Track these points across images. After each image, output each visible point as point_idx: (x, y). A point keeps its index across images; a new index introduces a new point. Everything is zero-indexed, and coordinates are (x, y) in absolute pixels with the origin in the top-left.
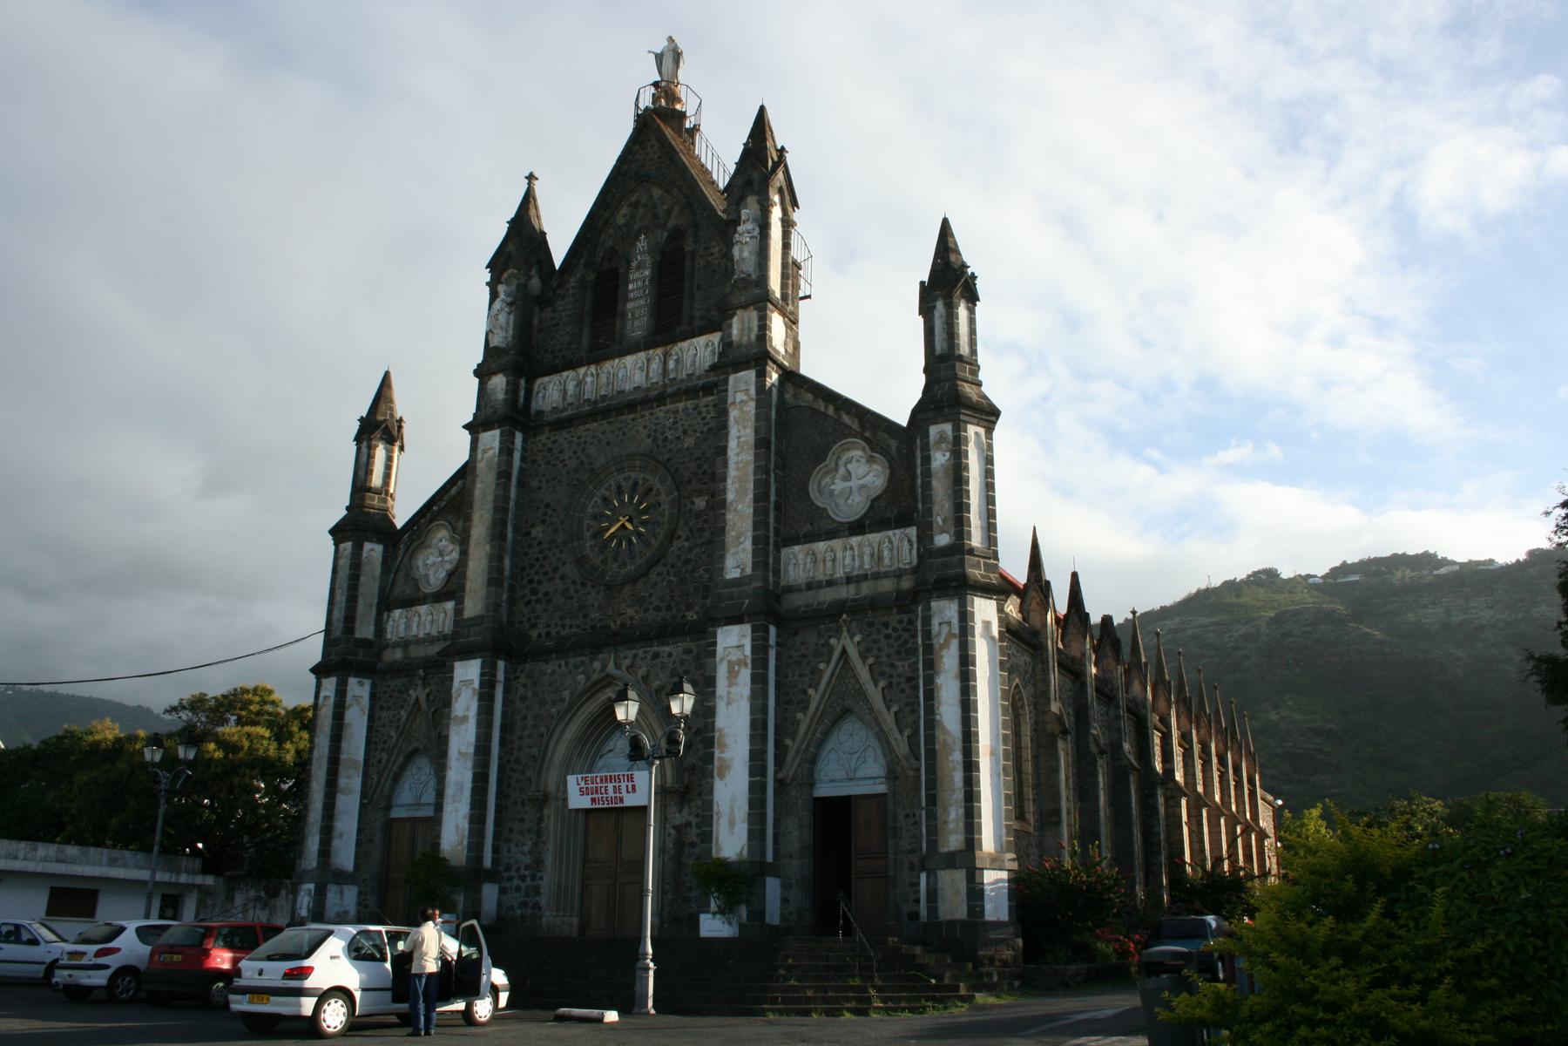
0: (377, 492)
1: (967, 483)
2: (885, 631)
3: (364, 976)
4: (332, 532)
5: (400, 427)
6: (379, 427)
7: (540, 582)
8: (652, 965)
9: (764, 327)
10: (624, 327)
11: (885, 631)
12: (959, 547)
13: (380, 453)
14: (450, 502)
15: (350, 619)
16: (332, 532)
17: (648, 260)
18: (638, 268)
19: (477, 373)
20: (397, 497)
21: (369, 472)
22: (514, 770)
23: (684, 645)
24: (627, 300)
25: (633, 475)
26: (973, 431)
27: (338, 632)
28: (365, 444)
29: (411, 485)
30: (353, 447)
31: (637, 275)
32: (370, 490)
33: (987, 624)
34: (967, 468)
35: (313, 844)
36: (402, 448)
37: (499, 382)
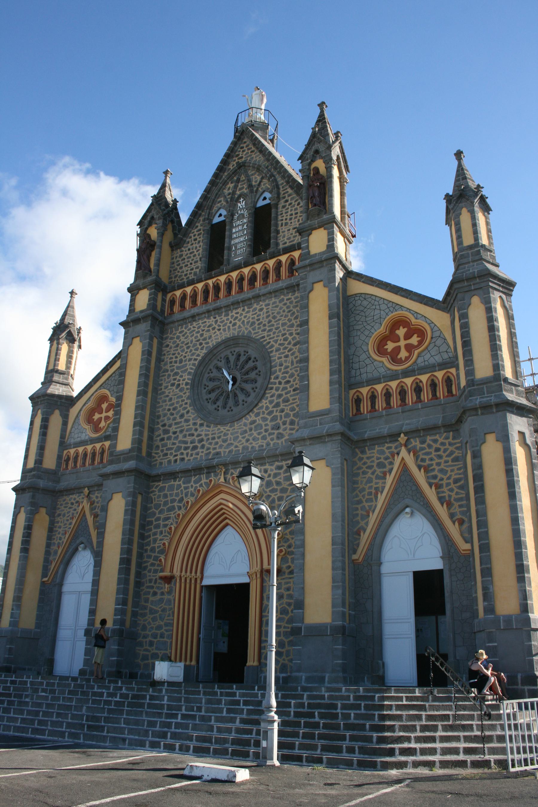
0: (62, 373)
1: (498, 330)
2: (435, 446)
3: (67, 159)
4: (32, 398)
5: (79, 333)
6: (64, 332)
7: (170, 426)
8: (276, 717)
9: (331, 239)
10: (229, 255)
11: (435, 446)
12: (497, 378)
13: (64, 348)
14: (113, 373)
15: (39, 461)
16: (32, 398)
17: (246, 213)
18: (238, 219)
19: (130, 290)
20: (75, 377)
21: (57, 359)
22: (149, 557)
23: (277, 463)
24: (231, 238)
25: (237, 350)
26: (496, 297)
27: (31, 464)
28: (55, 342)
29: (88, 363)
30: (47, 345)
31: (238, 223)
32: (57, 371)
33: (522, 434)
34: (497, 320)
35: (481, 605)
36: (80, 347)
37: (144, 297)
